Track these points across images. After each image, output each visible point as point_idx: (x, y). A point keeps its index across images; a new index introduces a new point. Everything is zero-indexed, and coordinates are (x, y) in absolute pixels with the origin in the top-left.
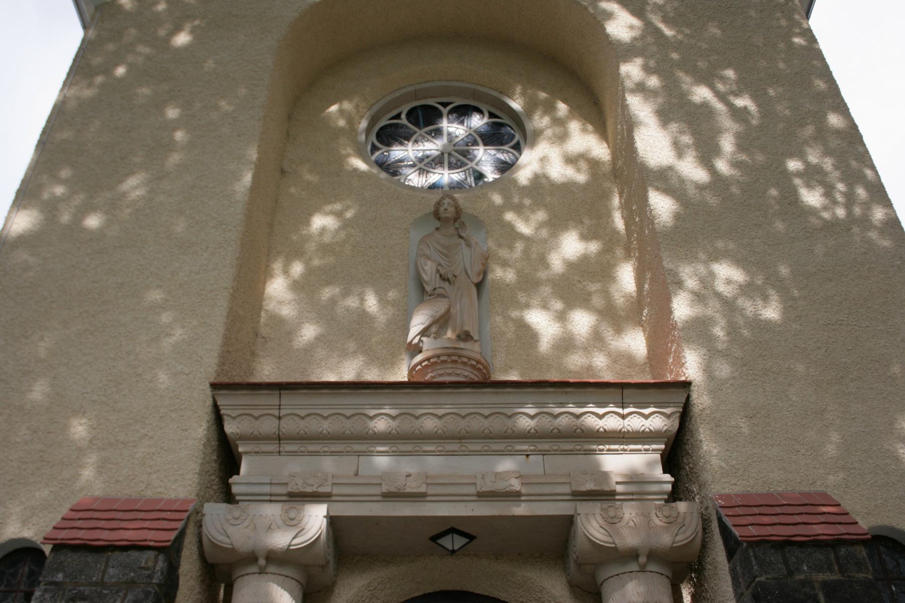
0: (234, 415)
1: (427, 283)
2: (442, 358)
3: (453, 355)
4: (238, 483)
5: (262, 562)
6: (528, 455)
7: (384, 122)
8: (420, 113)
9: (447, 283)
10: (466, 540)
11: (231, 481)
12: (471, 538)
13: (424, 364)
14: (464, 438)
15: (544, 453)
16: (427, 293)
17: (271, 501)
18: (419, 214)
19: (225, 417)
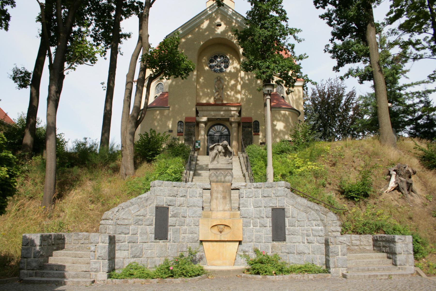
4: (199, 115)
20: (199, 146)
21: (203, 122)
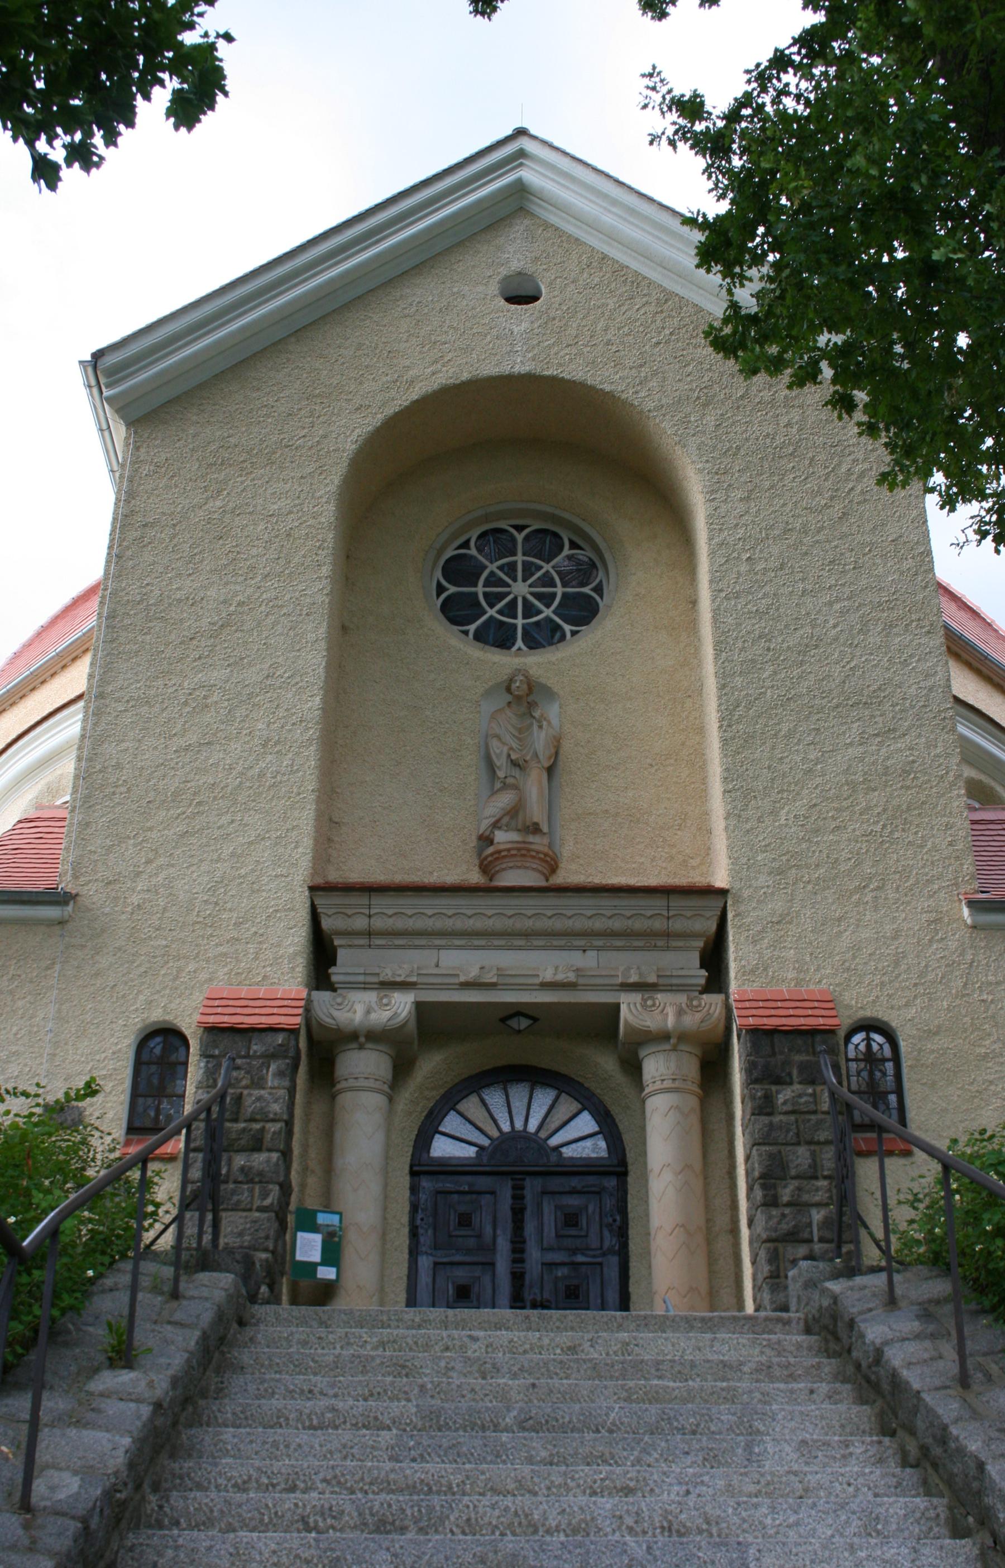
0: (330, 913)
1: (498, 768)
4: (337, 974)
5: (362, 1039)
6: (584, 951)
7: (449, 553)
9: (518, 769)
10: (529, 1022)
11: (330, 971)
12: (535, 1020)
14: (530, 935)
15: (599, 949)
17: (364, 988)
18: (490, 684)
19: (322, 916)
20: (326, 1262)
21: (374, 1037)
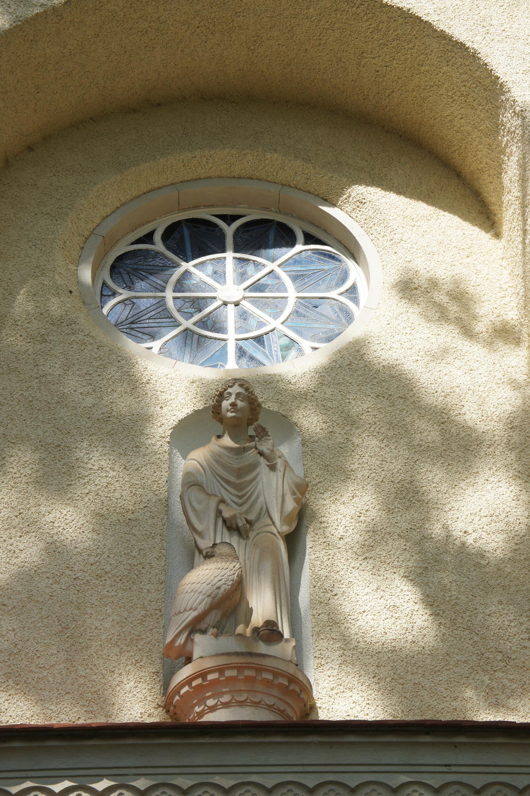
2: (229, 673)
3: (247, 668)
8: (186, 232)
13: (194, 684)
16: (200, 552)
